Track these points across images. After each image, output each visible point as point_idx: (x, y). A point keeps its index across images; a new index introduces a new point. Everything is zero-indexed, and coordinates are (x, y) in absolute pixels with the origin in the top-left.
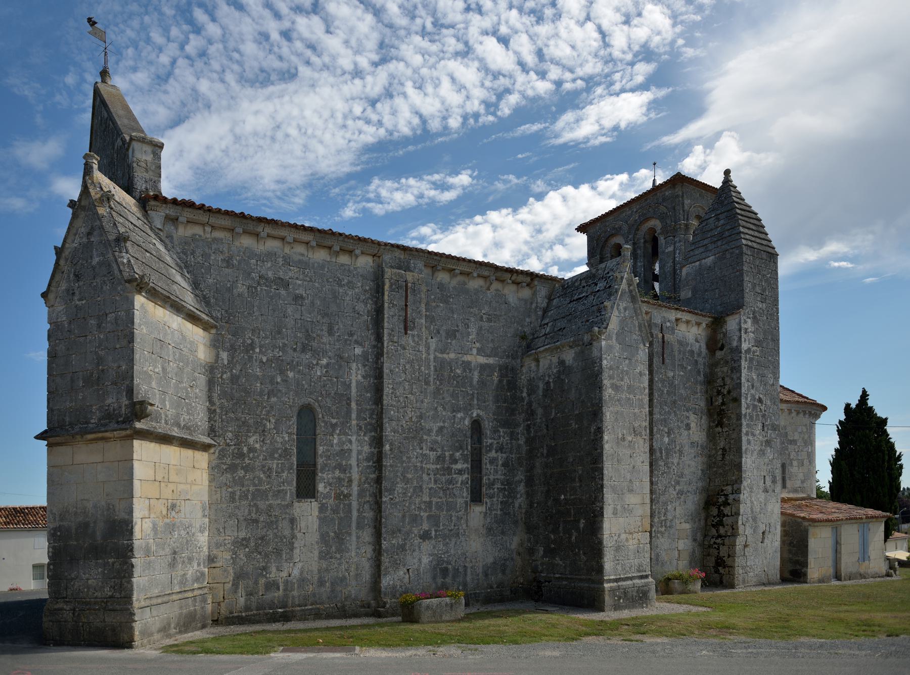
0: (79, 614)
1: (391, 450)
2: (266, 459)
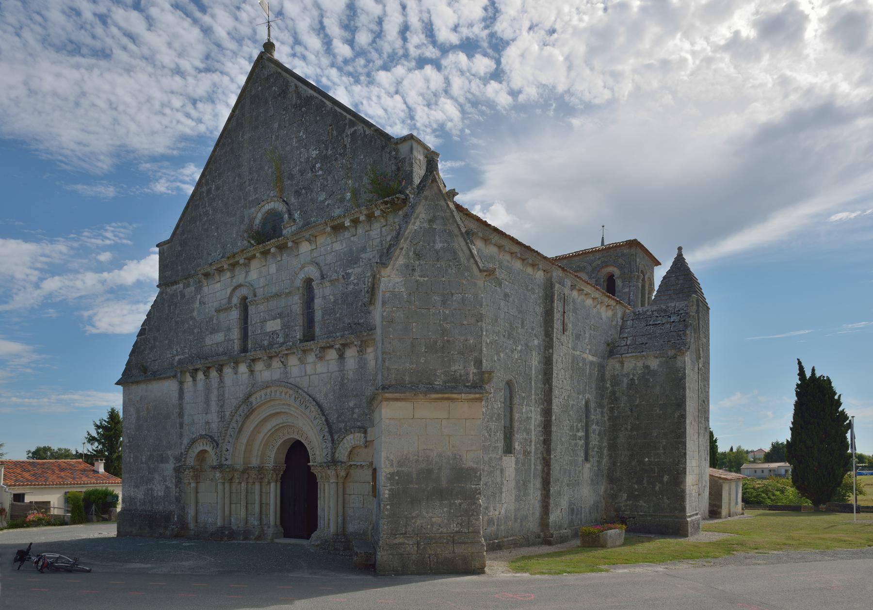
0: (424, 548)
1: (555, 419)
2: (488, 422)
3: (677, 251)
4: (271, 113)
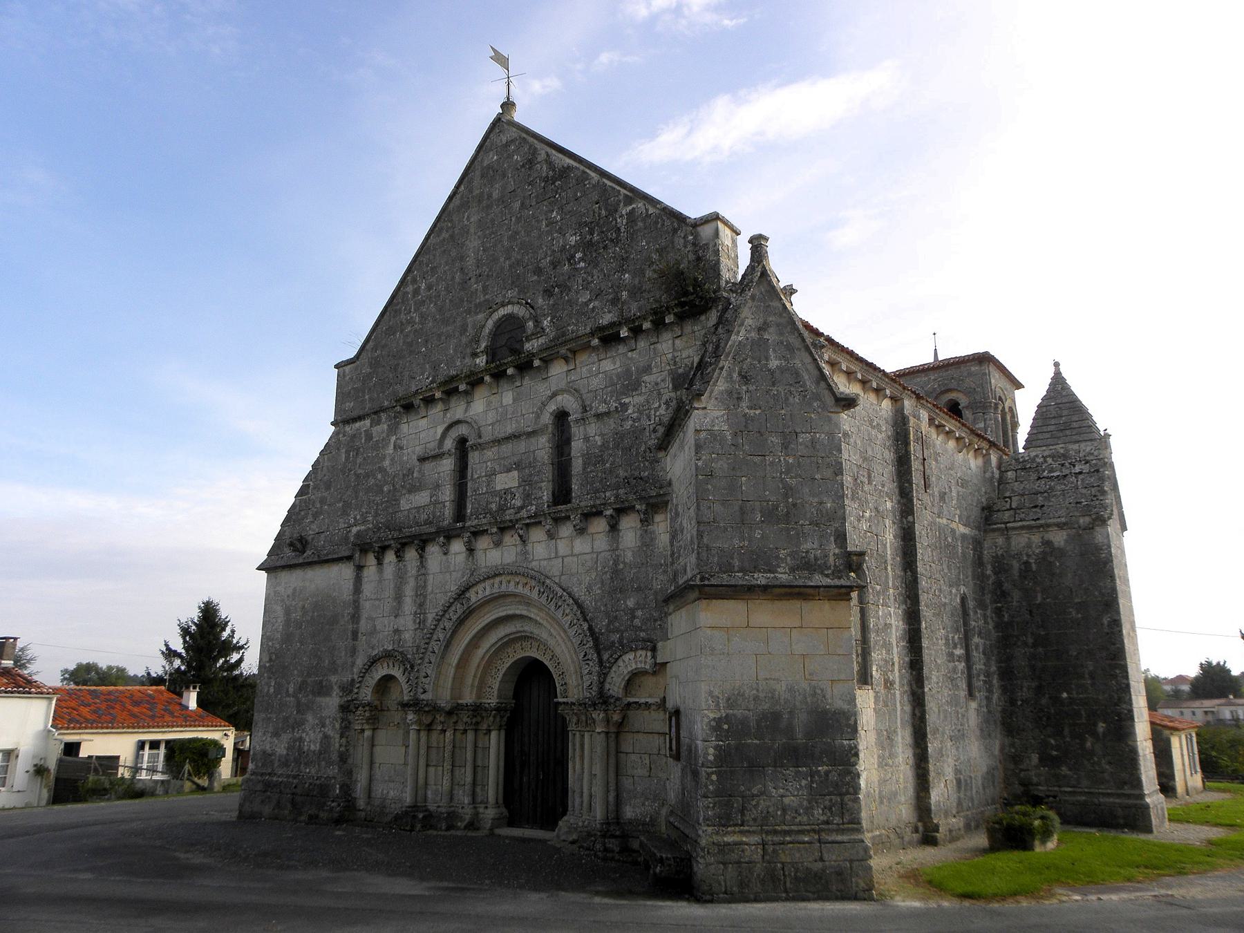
0: (774, 851)
3: (1053, 369)
4: (511, 187)
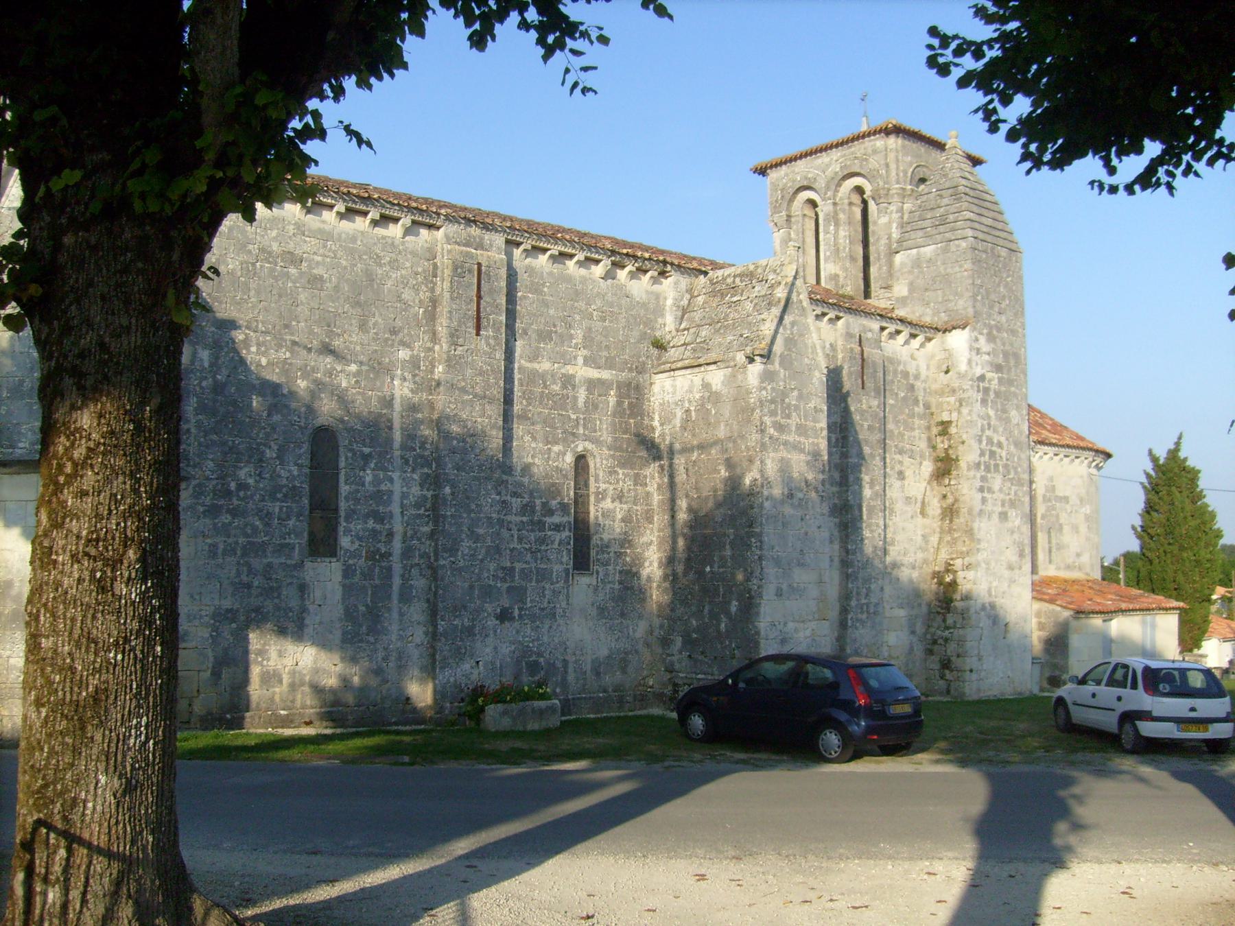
2: (263, 500)
